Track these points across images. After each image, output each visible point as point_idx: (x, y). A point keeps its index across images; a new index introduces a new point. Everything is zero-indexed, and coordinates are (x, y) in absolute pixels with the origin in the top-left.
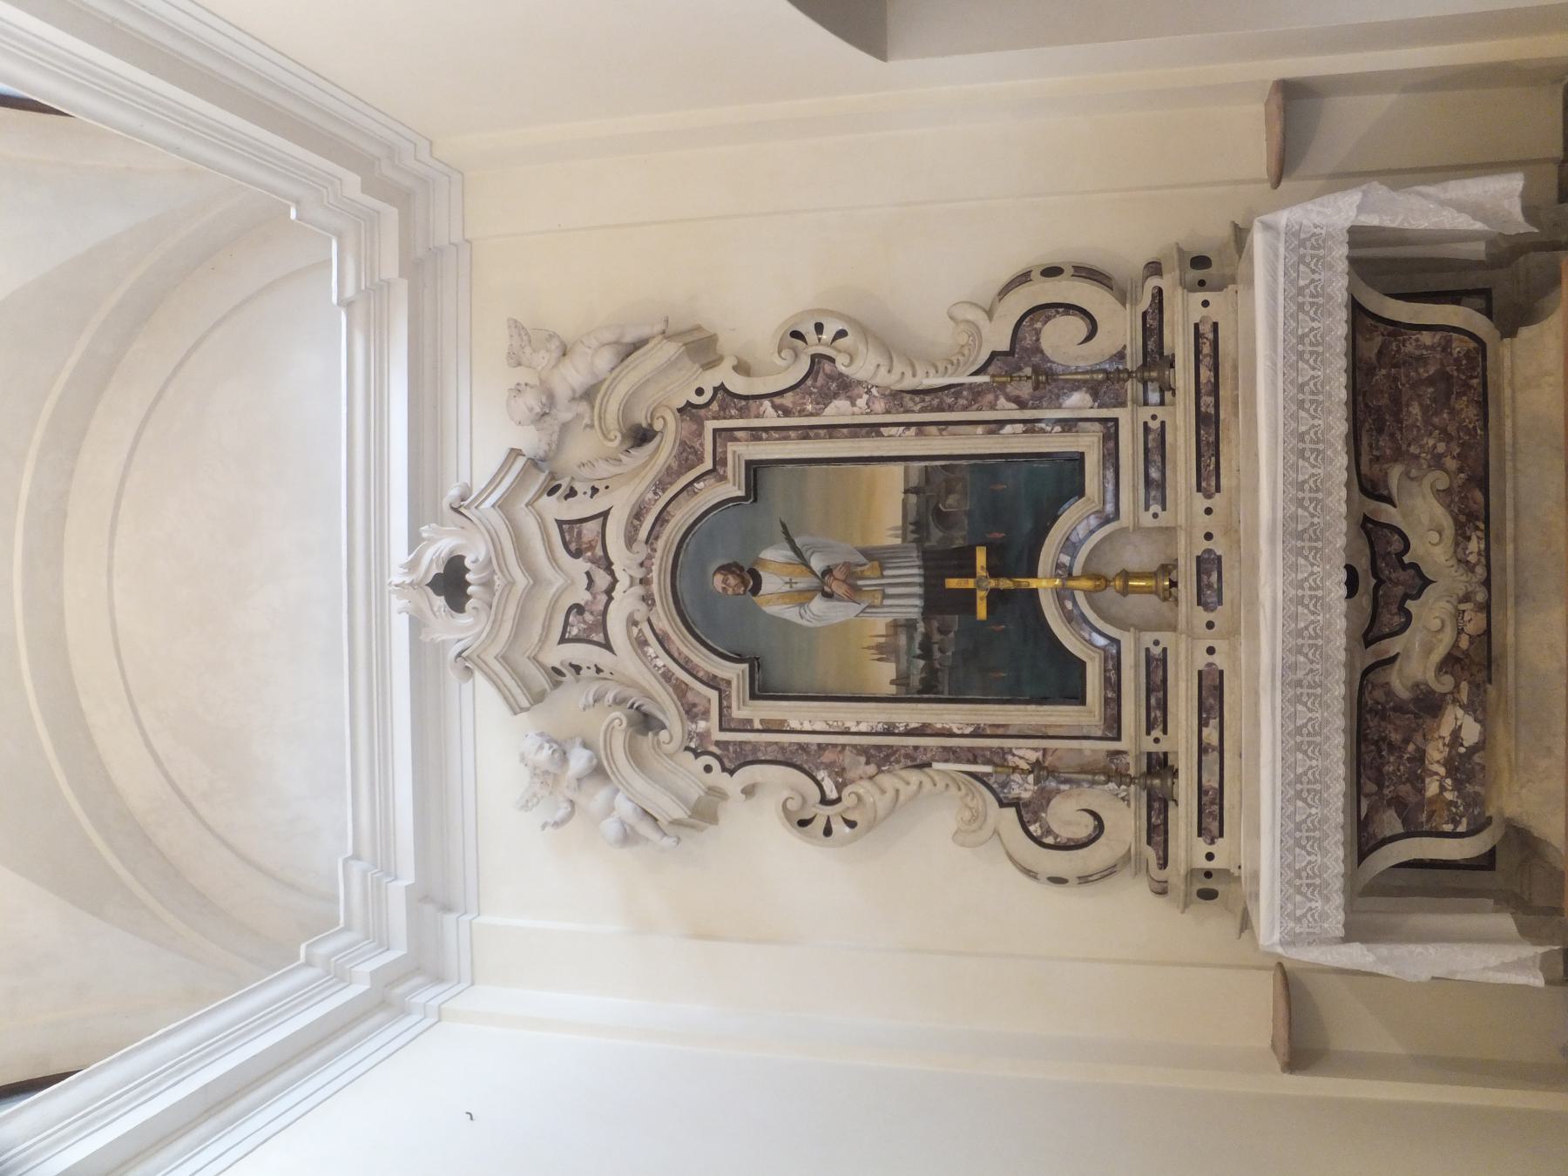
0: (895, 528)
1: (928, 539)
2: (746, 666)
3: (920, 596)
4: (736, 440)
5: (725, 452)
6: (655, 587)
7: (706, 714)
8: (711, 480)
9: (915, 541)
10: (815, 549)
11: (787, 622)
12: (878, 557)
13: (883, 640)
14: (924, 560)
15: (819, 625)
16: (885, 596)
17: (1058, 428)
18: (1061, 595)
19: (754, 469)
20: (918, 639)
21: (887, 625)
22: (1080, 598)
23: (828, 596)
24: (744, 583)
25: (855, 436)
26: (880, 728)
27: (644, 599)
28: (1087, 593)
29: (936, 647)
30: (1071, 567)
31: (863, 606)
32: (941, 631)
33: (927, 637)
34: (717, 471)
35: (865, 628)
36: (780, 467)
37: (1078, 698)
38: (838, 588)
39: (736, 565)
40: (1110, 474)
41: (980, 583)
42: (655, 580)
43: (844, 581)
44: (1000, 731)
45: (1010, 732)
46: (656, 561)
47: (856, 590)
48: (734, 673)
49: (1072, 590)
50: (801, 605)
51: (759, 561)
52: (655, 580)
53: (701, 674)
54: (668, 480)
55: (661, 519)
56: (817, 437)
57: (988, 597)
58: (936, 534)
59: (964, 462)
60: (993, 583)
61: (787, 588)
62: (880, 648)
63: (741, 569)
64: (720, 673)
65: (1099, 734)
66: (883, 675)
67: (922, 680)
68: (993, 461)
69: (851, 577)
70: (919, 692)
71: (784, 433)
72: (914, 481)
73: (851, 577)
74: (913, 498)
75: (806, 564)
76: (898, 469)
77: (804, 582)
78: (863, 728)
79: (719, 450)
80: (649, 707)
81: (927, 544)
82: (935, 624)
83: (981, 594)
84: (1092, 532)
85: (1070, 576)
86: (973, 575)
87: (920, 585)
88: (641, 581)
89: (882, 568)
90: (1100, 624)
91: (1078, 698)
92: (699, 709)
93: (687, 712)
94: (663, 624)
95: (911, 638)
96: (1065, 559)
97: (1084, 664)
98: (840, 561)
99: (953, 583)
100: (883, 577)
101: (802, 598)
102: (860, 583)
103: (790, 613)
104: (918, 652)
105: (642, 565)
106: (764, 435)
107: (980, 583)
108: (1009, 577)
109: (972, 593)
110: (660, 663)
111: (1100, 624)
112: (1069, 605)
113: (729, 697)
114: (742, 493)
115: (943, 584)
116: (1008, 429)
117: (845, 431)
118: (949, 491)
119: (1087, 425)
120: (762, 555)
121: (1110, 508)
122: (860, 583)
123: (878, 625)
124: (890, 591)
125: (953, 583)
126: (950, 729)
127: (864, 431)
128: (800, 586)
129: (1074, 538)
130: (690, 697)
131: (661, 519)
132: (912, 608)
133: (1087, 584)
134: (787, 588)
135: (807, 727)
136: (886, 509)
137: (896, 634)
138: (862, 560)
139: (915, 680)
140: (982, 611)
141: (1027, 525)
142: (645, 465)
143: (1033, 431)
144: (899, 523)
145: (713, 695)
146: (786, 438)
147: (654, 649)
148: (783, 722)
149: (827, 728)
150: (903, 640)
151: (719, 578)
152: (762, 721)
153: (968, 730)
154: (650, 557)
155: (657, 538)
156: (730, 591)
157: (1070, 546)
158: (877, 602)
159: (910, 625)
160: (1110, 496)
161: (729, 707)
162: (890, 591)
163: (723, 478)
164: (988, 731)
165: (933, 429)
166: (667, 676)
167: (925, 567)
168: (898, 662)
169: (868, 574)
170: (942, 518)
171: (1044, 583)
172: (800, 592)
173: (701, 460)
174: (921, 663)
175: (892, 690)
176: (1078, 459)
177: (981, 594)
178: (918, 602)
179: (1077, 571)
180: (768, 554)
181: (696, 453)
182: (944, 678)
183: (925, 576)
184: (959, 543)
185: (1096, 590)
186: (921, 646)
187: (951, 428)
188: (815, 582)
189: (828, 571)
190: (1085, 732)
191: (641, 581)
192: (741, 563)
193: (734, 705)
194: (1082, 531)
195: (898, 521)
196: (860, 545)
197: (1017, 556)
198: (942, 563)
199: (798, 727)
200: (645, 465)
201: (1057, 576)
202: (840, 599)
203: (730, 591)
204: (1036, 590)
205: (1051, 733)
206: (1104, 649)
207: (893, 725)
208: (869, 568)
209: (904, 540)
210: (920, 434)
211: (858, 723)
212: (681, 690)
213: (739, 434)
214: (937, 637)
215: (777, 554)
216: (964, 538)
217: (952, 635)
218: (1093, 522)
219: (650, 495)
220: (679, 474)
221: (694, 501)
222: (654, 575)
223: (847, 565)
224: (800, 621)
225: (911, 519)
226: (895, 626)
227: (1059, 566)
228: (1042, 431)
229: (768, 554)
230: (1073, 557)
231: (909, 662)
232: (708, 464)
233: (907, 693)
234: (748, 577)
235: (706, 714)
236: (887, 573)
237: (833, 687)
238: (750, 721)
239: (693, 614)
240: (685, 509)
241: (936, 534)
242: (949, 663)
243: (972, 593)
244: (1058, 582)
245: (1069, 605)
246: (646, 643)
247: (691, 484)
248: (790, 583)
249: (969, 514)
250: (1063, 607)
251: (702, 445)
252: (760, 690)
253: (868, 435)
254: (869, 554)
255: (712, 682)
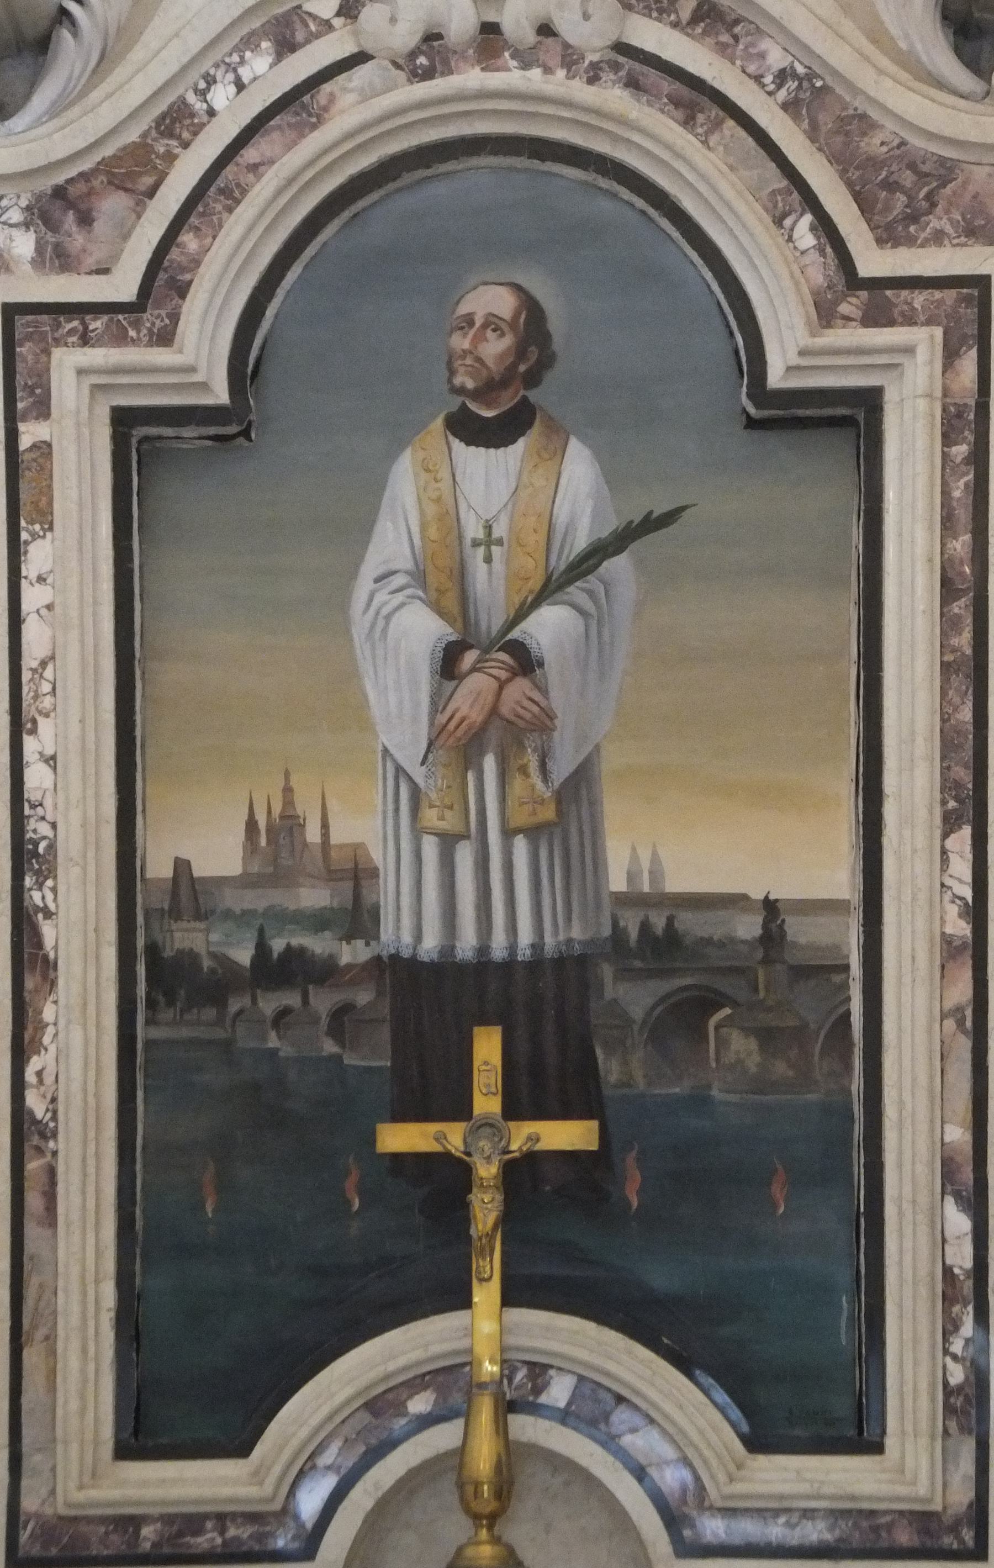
0: (656, 874)
1: (625, 973)
2: (221, 395)
3: (448, 950)
4: (951, 355)
5: (910, 320)
6: (471, 78)
7: (57, 258)
8: (819, 271)
9: (618, 934)
10: (595, 620)
11: (361, 529)
12: (568, 821)
13: (313, 834)
14: (560, 962)
15: (359, 631)
16: (448, 842)
17: (957, 1375)
18: (450, 1381)
19: (853, 419)
20: (318, 945)
21: (357, 849)
22: (444, 1437)
23: (448, 664)
24: (488, 389)
25: (948, 745)
26: (37, 828)
27: (432, 37)
28: (460, 1454)
29: (292, 999)
30: (534, 1409)
31: (419, 774)
32: (341, 1014)
33: (326, 973)
34: (852, 292)
35: (350, 780)
36: (854, 502)
37: (139, 1437)
38: (473, 694)
39: (546, 361)
40: (815, 1532)
41: (490, 1133)
42: (495, 80)
43: (494, 711)
44: (34, 1201)
45: (32, 1231)
46: (558, 83)
47: (468, 751)
48: (197, 355)
49: (466, 1413)
50: (419, 577)
51: (558, 435)
52: (495, 80)
53: (189, 240)
54: (826, 121)
55: (697, 99)
56: (949, 625)
57: (446, 1156)
58: (637, 998)
59: (857, 1084)
60: (487, 1171)
61: (473, 530)
62: (288, 826)
63: (532, 379)
64: (194, 308)
65: (29, 1503)
66: (204, 838)
67: (189, 959)
68: (859, 1160)
69: (511, 735)
70: (153, 950)
71: (963, 515)
72: (802, 932)
73: (511, 735)
74: (748, 927)
75: (549, 591)
76: (842, 882)
77: (491, 585)
78: (37, 777)
79: (919, 299)
80: (70, 56)
81: (607, 971)
82: (363, 997)
83: (454, 1136)
84: (640, 1473)
85: (508, 1407)
86: (514, 1109)
87: (483, 950)
88: (490, 29)
89: (534, 832)
90: (362, 1498)
91: (139, 1437)
92: (77, 240)
93: (59, 193)
94: (354, 108)
95: (319, 921)
96: (559, 1392)
97: (243, 1450)
98: (557, 700)
99: (488, 1048)
100: (508, 834)
101: (442, 577)
102: (490, 763)
103: (394, 540)
104: (277, 945)
105: (546, 30)
106: (961, 451)
107: (490, 1133)
108: (507, 1220)
109: (459, 1108)
110: (221, 96)
111: (362, 1498)
112: (420, 1404)
113: (121, 339)
114: (776, 378)
115: (485, 1021)
116: (959, 1222)
117: (966, 714)
118: (767, 1038)
119: (967, 1465)
120: (575, 447)
121: (713, 1528)
122: (490, 763)
123: (359, 822)
124: (465, 856)
125: (488, 1048)
126: (38, 1047)
127: (965, 776)
128: (479, 573)
129: (621, 1417)
130: (112, 205)
131: (697, 99)
132: (413, 924)
133: (483, 1457)
134: (473, 530)
135: (32, 598)
136: (717, 842)
137: (331, 875)
138: (562, 768)
139: (187, 937)
140: (400, 1138)
141: (662, 1276)
142: (877, 35)
143: (949, 1299)
144: (675, 884)
145: (123, 285)
146: (948, 523)
147: (268, 75)
148: (46, 519)
149: (29, 661)
150: (314, 897)
151: (493, 301)
152: (44, 449)
153: (35, 1103)
154: (570, 58)
155: (633, 84)
156: (461, 342)
157: (596, 1408)
158: (430, 817)
159: (358, 918)
160: (749, 1529)
161: (85, 340)
162: (465, 856)
163: (826, 314)
164: (33, 1166)
165: (962, 991)
166: (177, 122)
167: (536, 965)
168: (246, 881)
169: (518, 786)
170: (687, 1017)
171: (484, 1326)
172: (461, 575)
173: (888, 237)
174: (244, 956)
175: (157, 865)
176: (858, 1432)
177: (454, 1136)
178: (430, 944)
179: (525, 1428)
180: (579, 467)
181: (913, 217)
182: (198, 1025)
183: (509, 965)
184: (610, 1069)
185: (465, 1487)
186: (293, 955)
187: (964, 1046)
188: (492, 617)
189: (525, 662)
190: (32, 1460)
191: (490, 29)
192: (551, 379)
193: (97, 356)
194: (644, 1442)
195: (117, 350)
196: (610, 762)
197: (569, 1246)
198: (548, 1014)
199: (30, 569)
200: (877, 35)
201: (508, 1367)
202: (437, 703)
203: (461, 342)
204: (466, 1303)
205: (31, 1357)
206: (287, 1511)
207: (47, 871)
208: (532, 786)
209: (621, 900)
210: (950, 949)
211: (51, 761)
212: (133, 171)
213: (968, 365)
214: (323, 1002)
215: (580, 490)
216: (627, 1083)
217: (330, 1047)
218: (671, 1478)
219: (776, 58)
220: (843, 162)
221: (754, 217)
222: (512, 77)
223: (544, 723)
224: (370, 568)
225: (689, 923)
226: (358, 874)
227: (539, 1372)
228: (951, 1327)
229: (579, 467)
230: (564, 1417)
231: (245, 917)
232: (873, 261)
233: (148, 911)
234: (507, 401)
235: (57, 258)
236: (521, 845)
237: (163, 679)
238: (43, 409)
239: (387, 213)
240: (729, 187)
241: (637, 998)
242: (245, 1040)
243: (459, 1108)
244: (490, 1368)
245: (420, 1404)
246: (286, 47)
247: (811, 202)
248: (489, 541)
249: (699, 1101)
250: (416, 1384)
251: (938, 238)
252: (141, 440)
253: (949, 786)
254: (579, 790)
255: (165, 277)
